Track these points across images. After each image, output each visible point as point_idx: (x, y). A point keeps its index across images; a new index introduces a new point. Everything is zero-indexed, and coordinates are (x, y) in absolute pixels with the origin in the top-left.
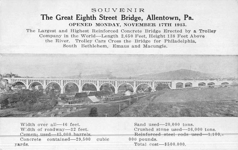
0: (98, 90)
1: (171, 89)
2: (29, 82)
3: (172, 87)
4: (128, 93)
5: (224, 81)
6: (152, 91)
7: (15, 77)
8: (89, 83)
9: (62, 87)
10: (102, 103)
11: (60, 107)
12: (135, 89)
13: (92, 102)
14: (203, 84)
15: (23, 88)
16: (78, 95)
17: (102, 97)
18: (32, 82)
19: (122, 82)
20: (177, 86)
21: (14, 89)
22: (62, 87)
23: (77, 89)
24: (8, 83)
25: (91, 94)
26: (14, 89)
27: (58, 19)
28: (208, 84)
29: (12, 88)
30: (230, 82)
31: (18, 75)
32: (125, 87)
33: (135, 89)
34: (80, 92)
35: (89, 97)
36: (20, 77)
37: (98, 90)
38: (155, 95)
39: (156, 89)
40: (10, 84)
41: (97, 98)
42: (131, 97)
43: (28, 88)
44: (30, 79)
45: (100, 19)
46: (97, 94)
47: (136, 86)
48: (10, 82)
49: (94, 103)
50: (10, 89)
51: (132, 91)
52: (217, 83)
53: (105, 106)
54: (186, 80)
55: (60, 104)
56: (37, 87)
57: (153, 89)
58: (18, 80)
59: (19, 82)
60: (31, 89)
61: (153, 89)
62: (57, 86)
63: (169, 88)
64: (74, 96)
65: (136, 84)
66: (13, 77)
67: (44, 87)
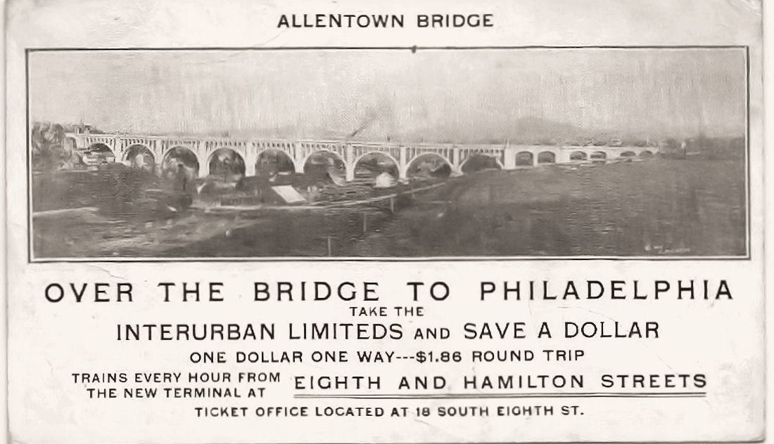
0: (299, 168)
1: (503, 167)
2: (122, 145)
3: (506, 165)
4: (384, 181)
5: (625, 149)
6: (452, 175)
7: (91, 132)
8: (275, 150)
9: (204, 158)
10: (312, 207)
11: (199, 212)
12: (403, 169)
13: (283, 202)
14: (581, 156)
15: (110, 159)
16: (244, 184)
17: (311, 188)
18: (133, 143)
19: (365, 148)
20: (520, 162)
21: (90, 160)
22: (204, 158)
23: (242, 168)
24: (75, 146)
25: (281, 182)
26: (90, 160)
27: (324, 286)
28: (592, 157)
29: (85, 159)
30: (638, 151)
31: (99, 128)
32: (371, 166)
33: (403, 169)
34: (247, 174)
35: (275, 189)
36: (101, 133)
37: (299, 168)
38: (463, 184)
39: (463, 169)
40: (81, 149)
41: (299, 192)
42: (397, 188)
43: (118, 160)
44: (165, 138)
46: (297, 182)
47: (408, 160)
48: (79, 145)
49: (291, 205)
50: (81, 161)
51: (393, 171)
52: (613, 154)
53: (320, 216)
54: (578, 145)
55: (198, 204)
56: (140, 158)
57: (457, 169)
58: (99, 139)
59: (98, 145)
60: (127, 163)
61: (457, 169)
62: (190, 159)
63: (498, 167)
64: (234, 185)
65: (408, 155)
66: (87, 132)
67: (159, 157)
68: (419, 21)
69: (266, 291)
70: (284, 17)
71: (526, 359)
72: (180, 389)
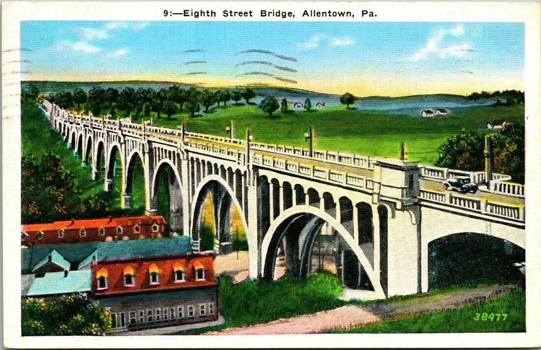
45: (224, 16)
68: (262, 13)
69: (265, 13)
70: (306, 11)
71: (285, 13)
72: (188, 11)
